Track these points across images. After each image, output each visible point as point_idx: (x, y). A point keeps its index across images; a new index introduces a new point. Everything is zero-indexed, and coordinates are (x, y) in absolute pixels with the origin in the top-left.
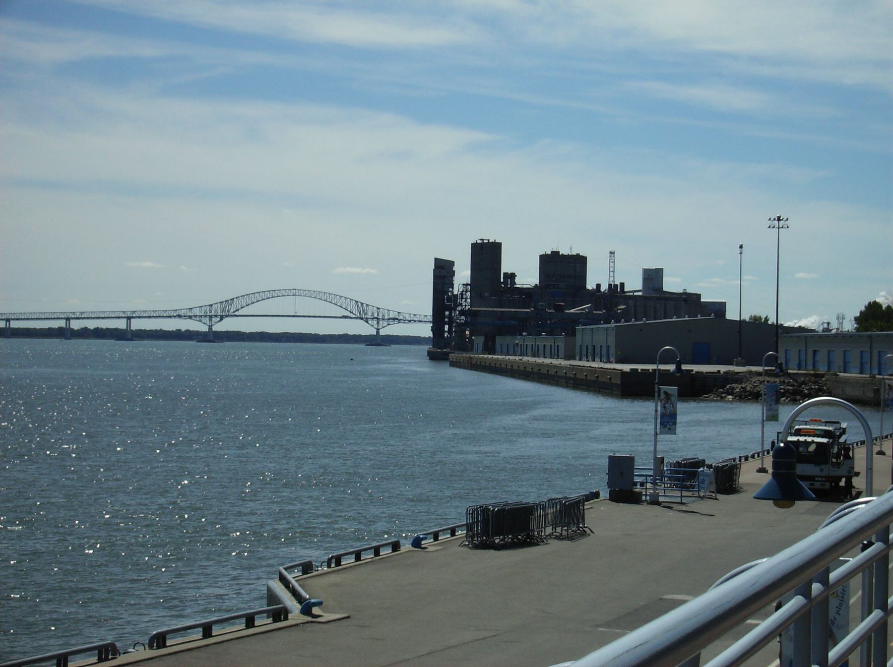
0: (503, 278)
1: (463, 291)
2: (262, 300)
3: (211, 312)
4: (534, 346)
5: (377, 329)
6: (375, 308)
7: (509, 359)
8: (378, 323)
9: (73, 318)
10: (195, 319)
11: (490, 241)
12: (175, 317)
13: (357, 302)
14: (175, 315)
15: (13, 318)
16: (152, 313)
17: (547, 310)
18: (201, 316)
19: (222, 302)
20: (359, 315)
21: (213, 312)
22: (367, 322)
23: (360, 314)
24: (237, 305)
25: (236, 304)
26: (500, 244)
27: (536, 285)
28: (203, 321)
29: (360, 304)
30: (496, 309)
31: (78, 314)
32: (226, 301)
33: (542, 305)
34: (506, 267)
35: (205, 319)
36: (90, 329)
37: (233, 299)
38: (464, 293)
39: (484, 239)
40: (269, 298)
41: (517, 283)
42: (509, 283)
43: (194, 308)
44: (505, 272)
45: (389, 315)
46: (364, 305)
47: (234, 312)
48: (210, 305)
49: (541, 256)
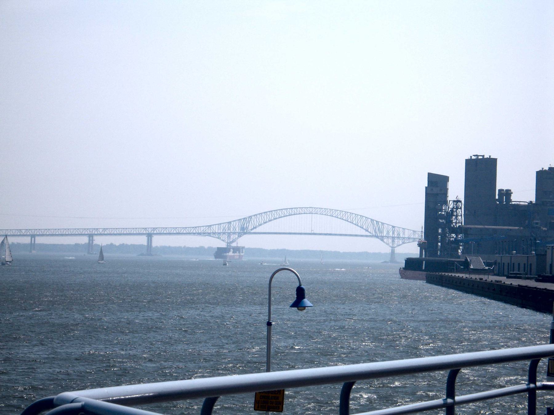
0: (498, 195)
1: (453, 208)
2: (279, 218)
3: (229, 229)
4: (526, 265)
5: (392, 247)
6: (390, 227)
7: (459, 276)
8: (393, 241)
9: (96, 235)
10: (214, 236)
11: (485, 157)
12: (194, 234)
13: (372, 220)
14: (194, 232)
15: (38, 233)
16: (172, 231)
17: (542, 228)
18: (220, 233)
19: (240, 220)
20: (374, 233)
21: (232, 229)
22: (382, 240)
23: (376, 232)
24: (255, 220)
25: (254, 222)
26: (495, 160)
27: (531, 202)
28: (222, 238)
29: (380, 223)
30: (486, 227)
31: (101, 230)
32: (244, 219)
33: (537, 223)
34: (501, 184)
35: (224, 236)
36: (115, 245)
37: (251, 217)
38: (455, 210)
39: (478, 155)
40: (281, 217)
41: (513, 200)
42: (504, 201)
43: (213, 225)
44: (500, 188)
45: (404, 234)
46: (380, 223)
47: (251, 230)
48: (228, 223)
49: (537, 172)
